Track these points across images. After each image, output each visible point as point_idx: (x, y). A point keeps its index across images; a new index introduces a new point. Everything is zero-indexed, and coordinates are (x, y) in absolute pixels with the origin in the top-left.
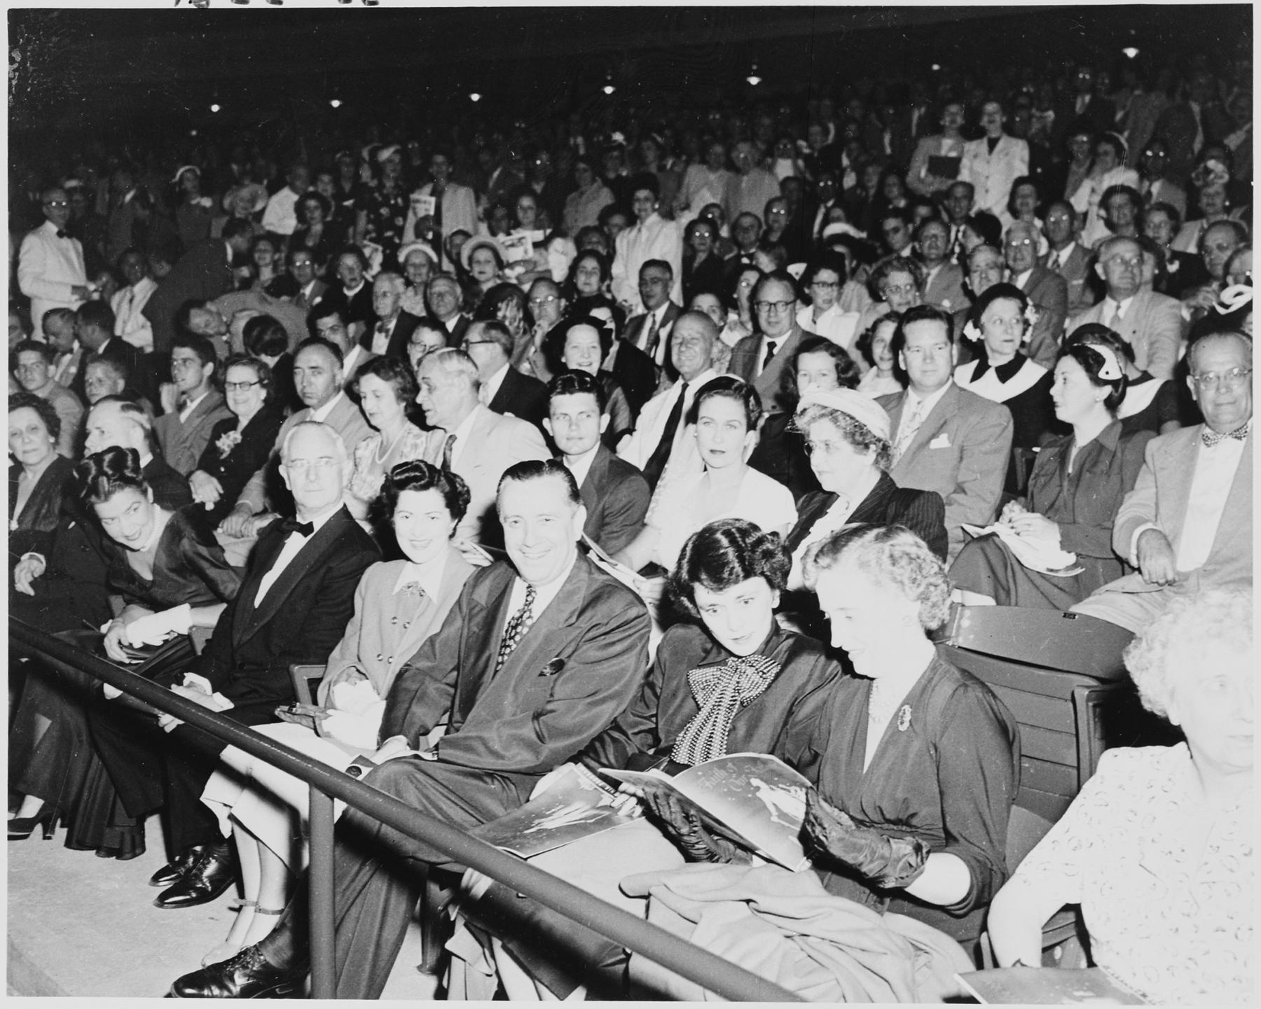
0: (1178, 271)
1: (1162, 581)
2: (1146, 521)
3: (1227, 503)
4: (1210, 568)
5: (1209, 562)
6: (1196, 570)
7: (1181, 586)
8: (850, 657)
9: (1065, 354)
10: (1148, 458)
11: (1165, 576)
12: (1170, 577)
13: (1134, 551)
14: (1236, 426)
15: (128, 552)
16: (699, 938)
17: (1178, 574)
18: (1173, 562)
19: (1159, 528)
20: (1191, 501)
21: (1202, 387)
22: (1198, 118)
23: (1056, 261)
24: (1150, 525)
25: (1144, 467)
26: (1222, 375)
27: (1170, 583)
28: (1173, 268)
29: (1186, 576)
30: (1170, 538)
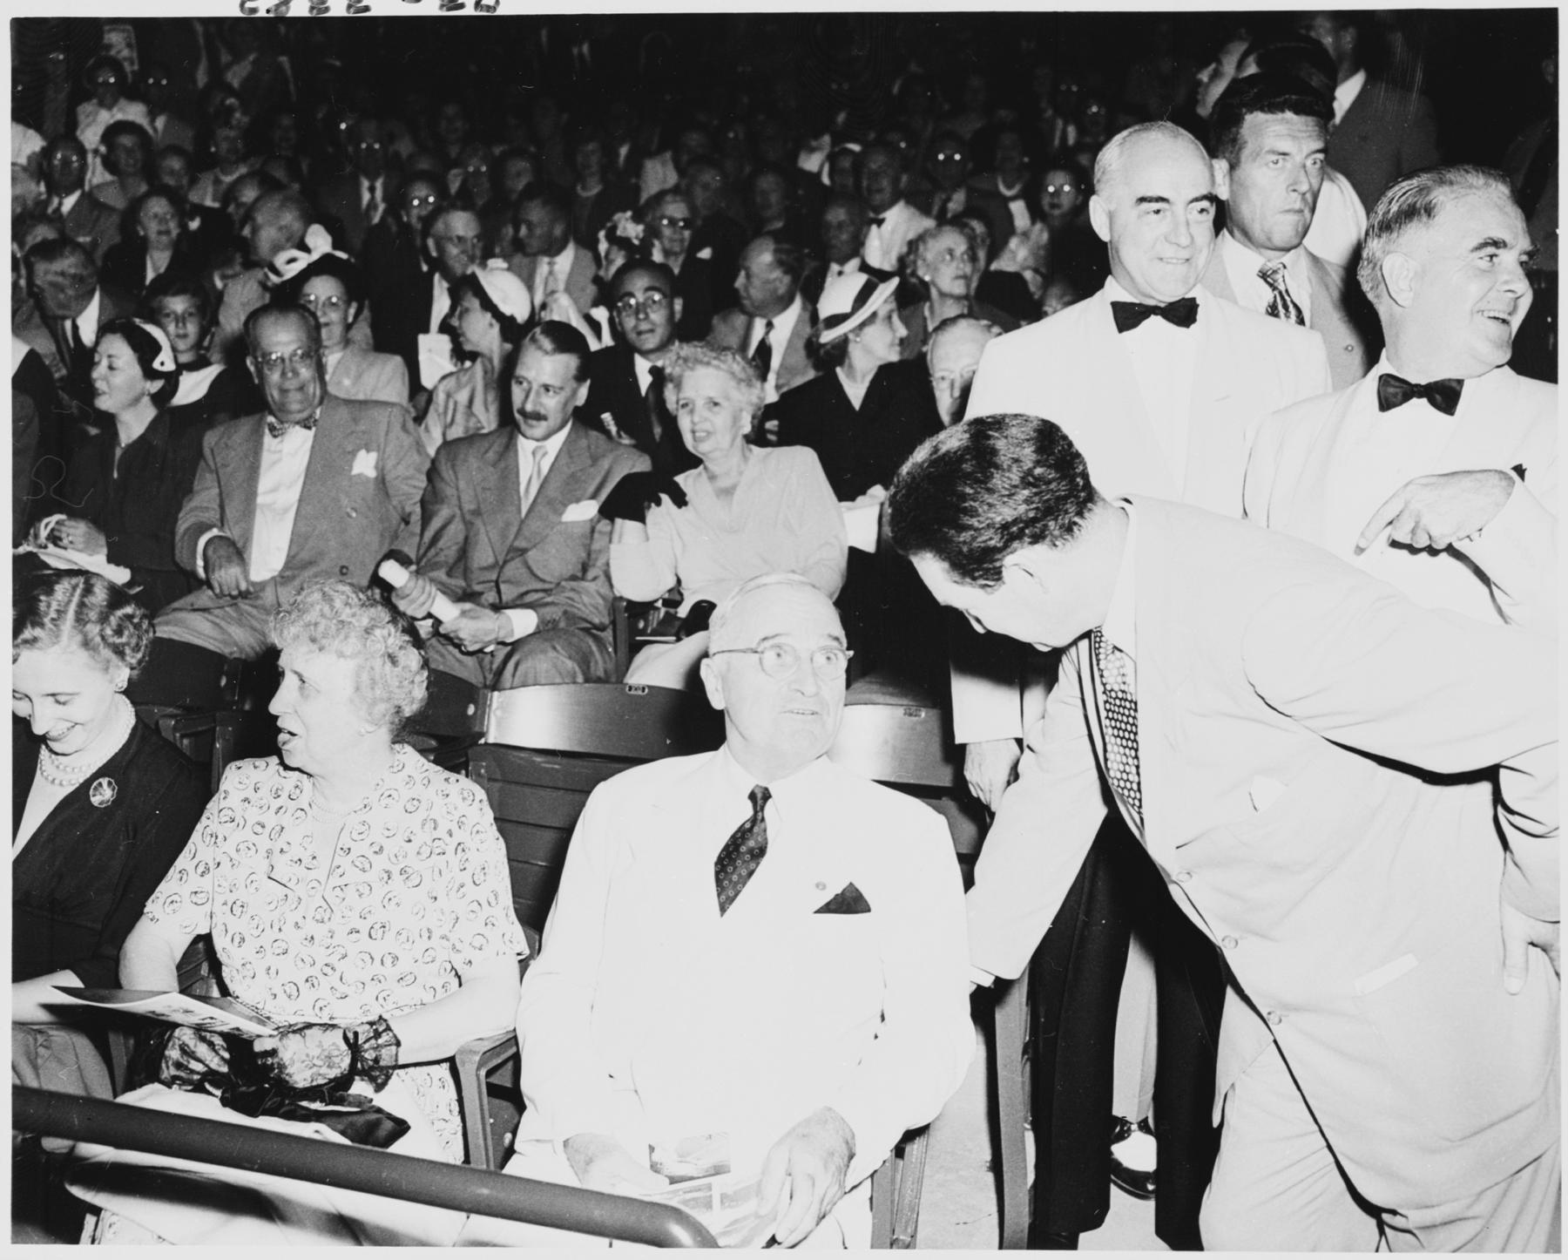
0: (199, 228)
1: (235, 593)
2: (209, 527)
3: (300, 501)
4: (288, 573)
5: (288, 565)
6: (273, 578)
7: (257, 598)
8: (241, 782)
9: (114, 331)
10: (207, 451)
11: (238, 587)
12: (243, 586)
13: (200, 563)
14: (305, 415)
15: (1230, 992)
16: (597, 1181)
17: (254, 584)
18: (246, 573)
19: (228, 534)
20: (260, 500)
21: (266, 371)
22: (289, 72)
23: (58, 209)
24: (215, 532)
25: (202, 463)
26: (286, 356)
27: (244, 595)
28: (194, 225)
29: (262, 586)
30: (240, 545)
